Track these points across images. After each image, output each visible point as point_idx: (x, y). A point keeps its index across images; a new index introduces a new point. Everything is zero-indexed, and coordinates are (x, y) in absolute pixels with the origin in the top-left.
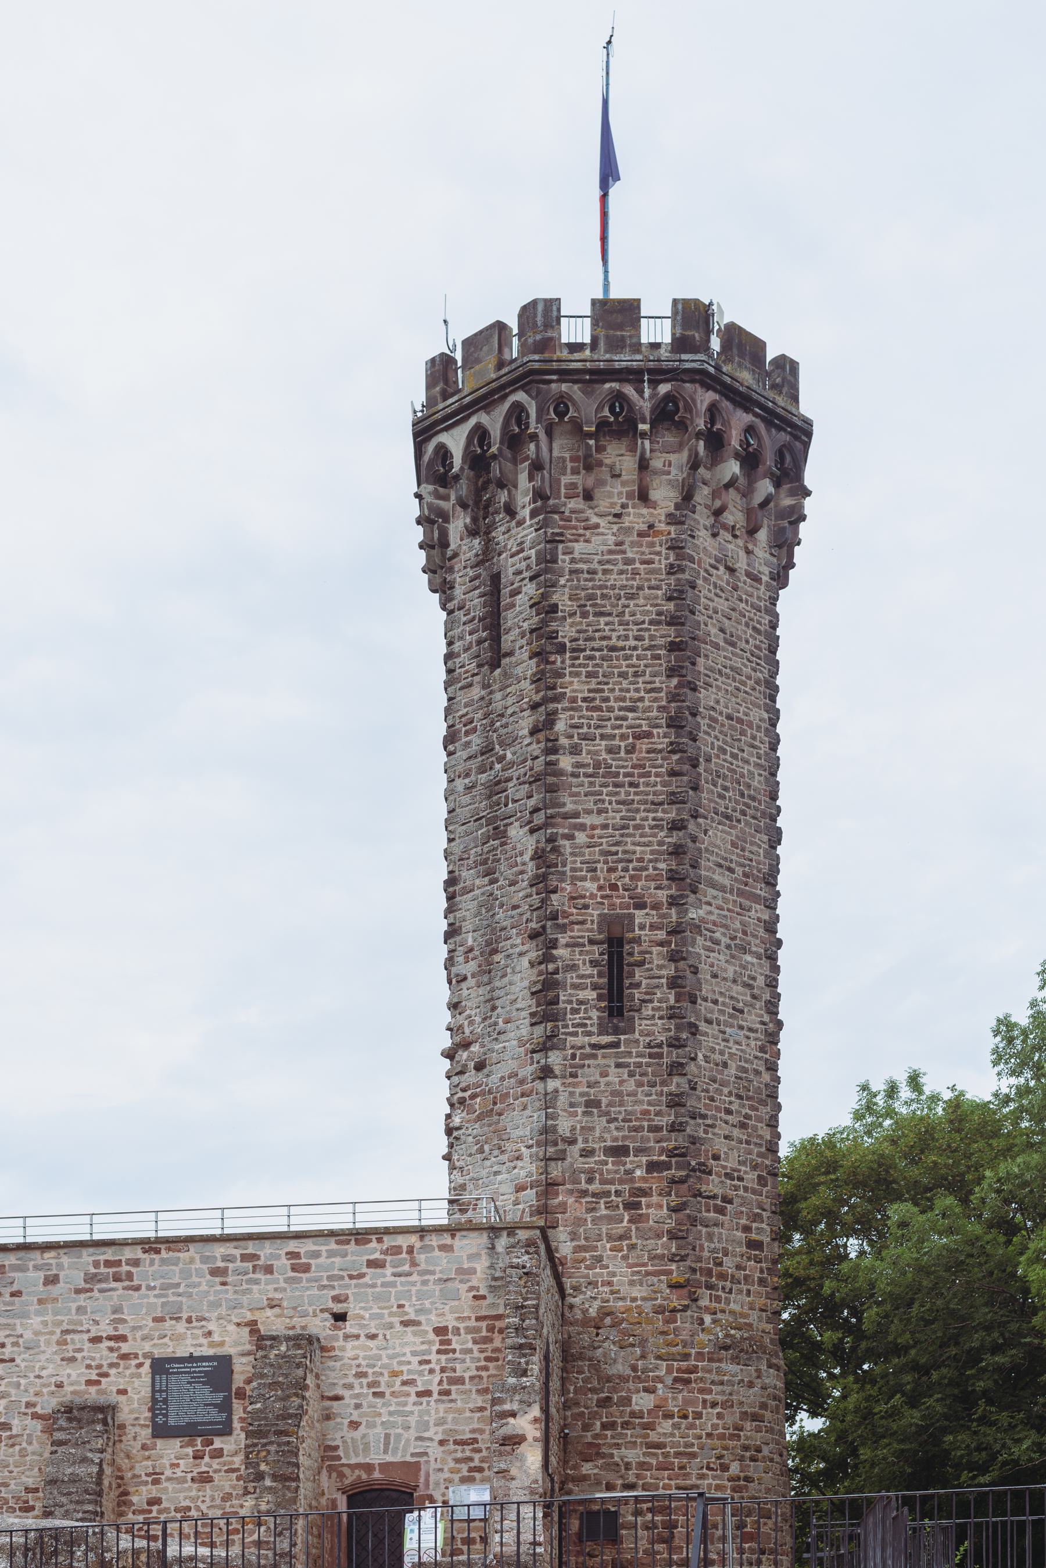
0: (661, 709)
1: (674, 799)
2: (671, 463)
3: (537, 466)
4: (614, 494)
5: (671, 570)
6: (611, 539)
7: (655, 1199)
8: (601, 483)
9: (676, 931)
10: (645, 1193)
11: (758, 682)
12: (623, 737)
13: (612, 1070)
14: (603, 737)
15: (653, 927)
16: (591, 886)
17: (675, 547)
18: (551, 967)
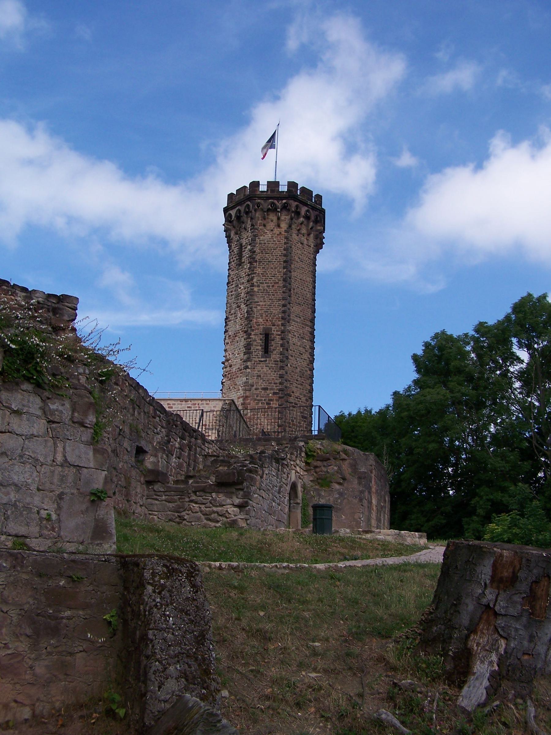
0: (281, 277)
1: (284, 299)
2: (285, 218)
3: (252, 219)
4: (271, 225)
5: (285, 243)
6: (270, 236)
7: (275, 402)
8: (268, 223)
9: (283, 332)
10: (271, 400)
11: (309, 271)
12: (271, 283)
13: (265, 367)
14: (266, 283)
15: (277, 331)
16: (261, 320)
17: (286, 238)
18: (249, 340)
